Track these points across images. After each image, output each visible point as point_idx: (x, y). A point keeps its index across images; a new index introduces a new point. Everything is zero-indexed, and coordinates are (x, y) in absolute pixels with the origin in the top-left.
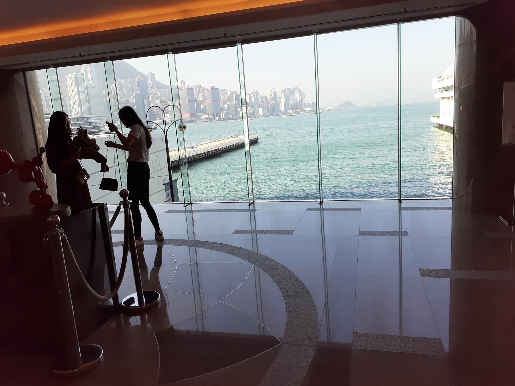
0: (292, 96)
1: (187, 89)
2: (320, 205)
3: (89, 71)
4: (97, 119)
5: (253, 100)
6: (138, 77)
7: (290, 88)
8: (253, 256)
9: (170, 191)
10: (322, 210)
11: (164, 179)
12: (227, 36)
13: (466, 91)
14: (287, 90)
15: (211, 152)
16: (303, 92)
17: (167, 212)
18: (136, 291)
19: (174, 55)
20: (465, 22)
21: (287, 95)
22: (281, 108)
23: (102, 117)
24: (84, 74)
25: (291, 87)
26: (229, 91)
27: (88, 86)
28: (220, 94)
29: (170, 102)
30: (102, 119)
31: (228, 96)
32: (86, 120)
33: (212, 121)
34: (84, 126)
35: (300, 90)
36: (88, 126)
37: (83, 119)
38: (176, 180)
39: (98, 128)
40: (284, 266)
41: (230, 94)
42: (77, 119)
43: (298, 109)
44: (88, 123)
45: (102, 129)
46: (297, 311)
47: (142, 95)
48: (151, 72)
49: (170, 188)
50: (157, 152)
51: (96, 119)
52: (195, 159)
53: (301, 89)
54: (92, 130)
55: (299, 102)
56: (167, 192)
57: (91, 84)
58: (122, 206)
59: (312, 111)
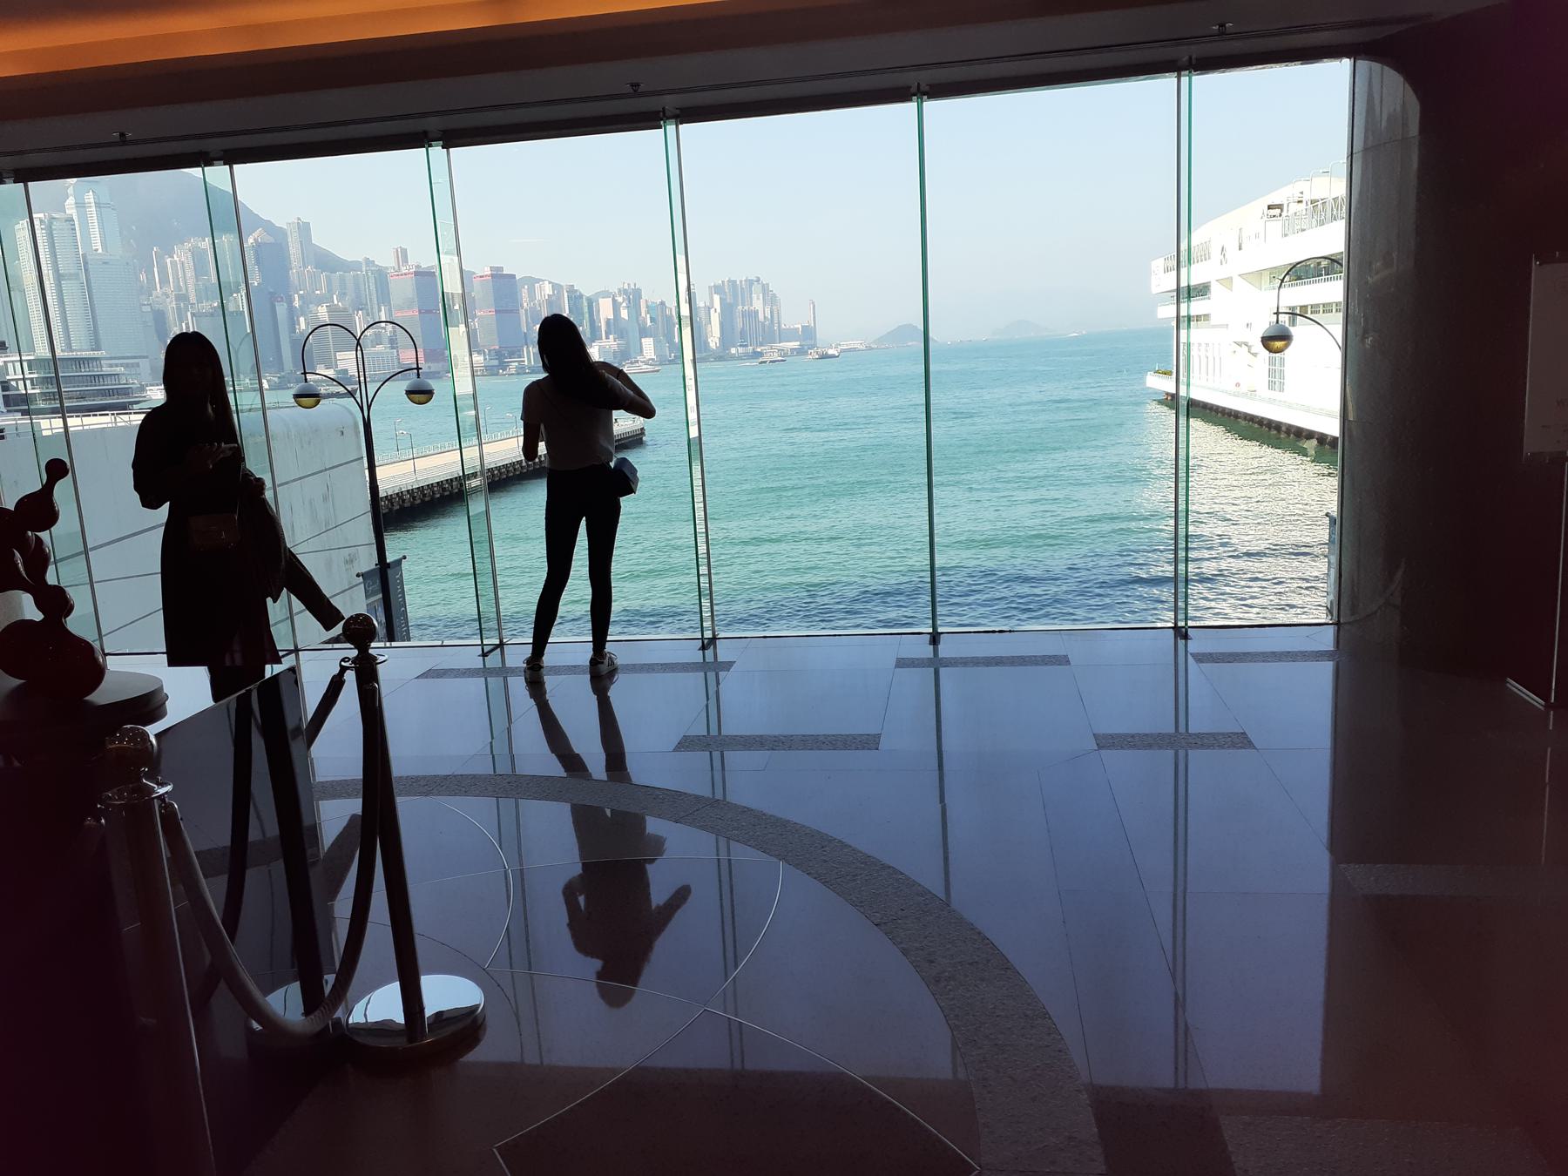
0: (743, 305)
1: (416, 273)
2: (932, 646)
3: (94, 209)
4: (122, 365)
5: (624, 314)
6: (255, 234)
7: (735, 281)
8: (771, 831)
9: (381, 596)
10: (936, 663)
11: (348, 558)
12: (639, 91)
13: (1393, 289)
14: (726, 287)
15: (496, 472)
16: (774, 295)
17: (424, 675)
18: (397, 977)
19: (448, 153)
20: (1382, 79)
21: (728, 301)
22: (709, 340)
23: (135, 357)
24: (75, 218)
25: (739, 277)
26: (550, 283)
27: (89, 257)
28: (521, 291)
29: (360, 312)
30: (138, 365)
31: (547, 297)
32: (82, 366)
33: (497, 374)
34: (78, 387)
35: (765, 289)
36: (91, 386)
37: (73, 362)
38: (398, 562)
39: (125, 392)
40: (890, 867)
41: (551, 293)
42: (81, 362)
43: (761, 345)
44: (90, 376)
45: (136, 397)
46: (993, 1037)
47: (271, 290)
48: (299, 219)
49: (380, 588)
50: (326, 470)
51: (117, 366)
52: (446, 493)
53: (768, 284)
54: (106, 400)
55: (763, 324)
56: (372, 599)
57: (100, 251)
58: (350, 676)
59: (809, 351)
